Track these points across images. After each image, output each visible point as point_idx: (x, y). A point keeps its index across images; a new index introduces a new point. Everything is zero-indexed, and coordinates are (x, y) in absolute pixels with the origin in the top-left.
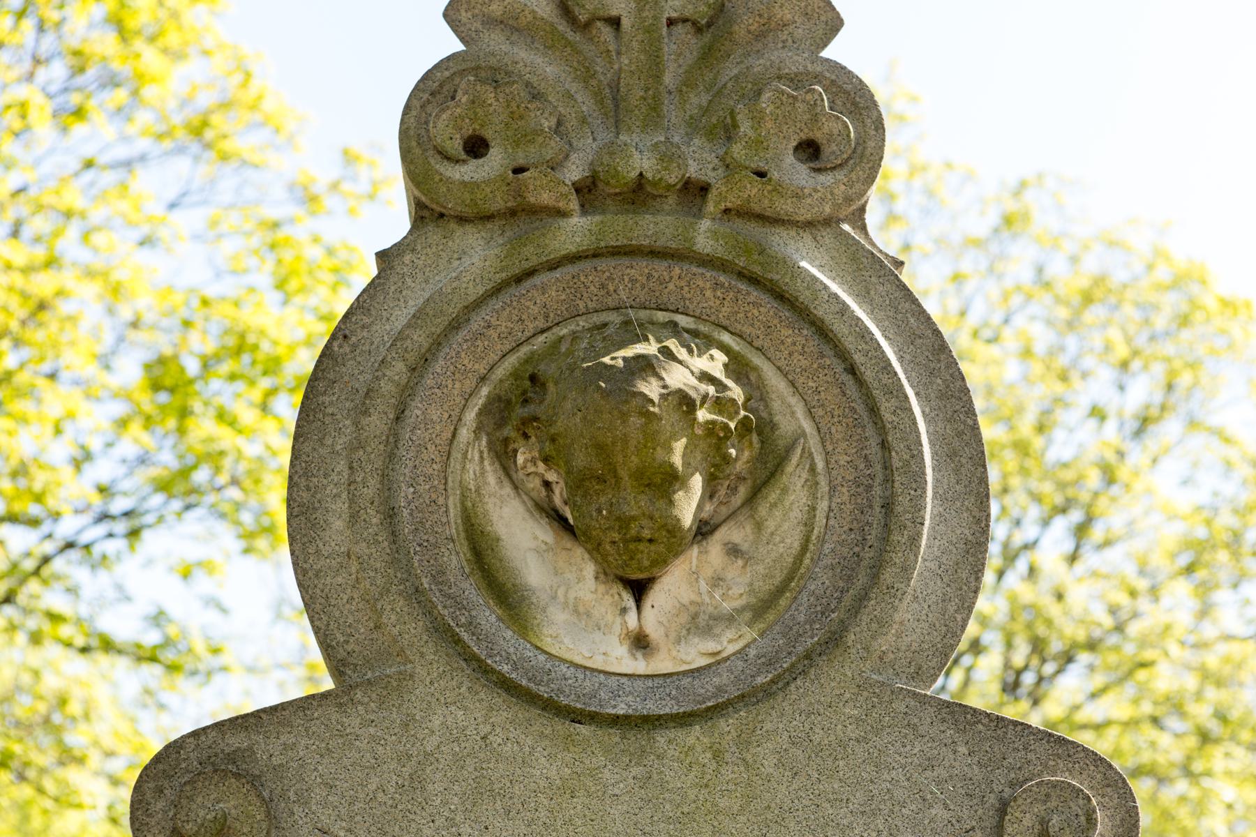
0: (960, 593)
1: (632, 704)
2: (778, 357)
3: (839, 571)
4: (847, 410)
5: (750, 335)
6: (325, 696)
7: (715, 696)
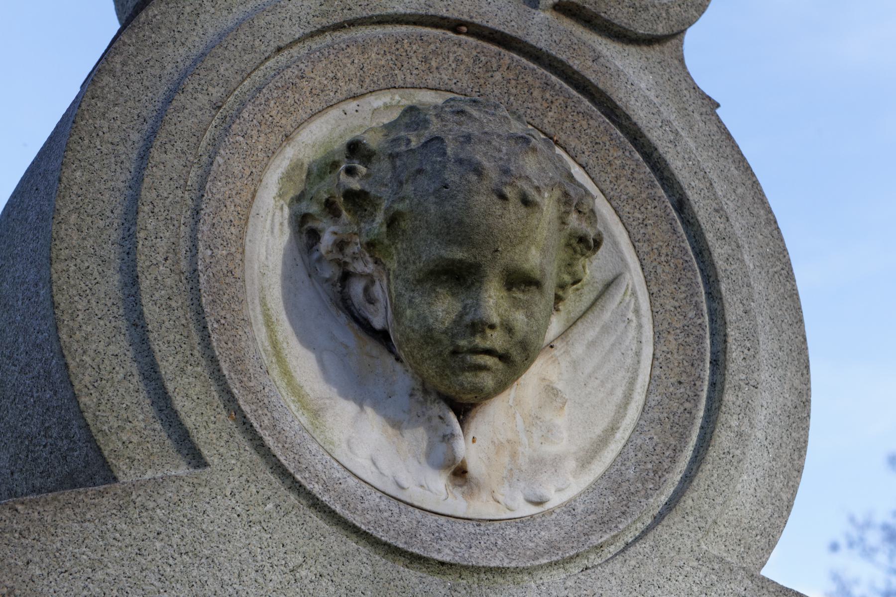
0: (784, 469)
1: (458, 550)
2: (603, 179)
3: (668, 426)
4: (676, 249)
5: (574, 149)
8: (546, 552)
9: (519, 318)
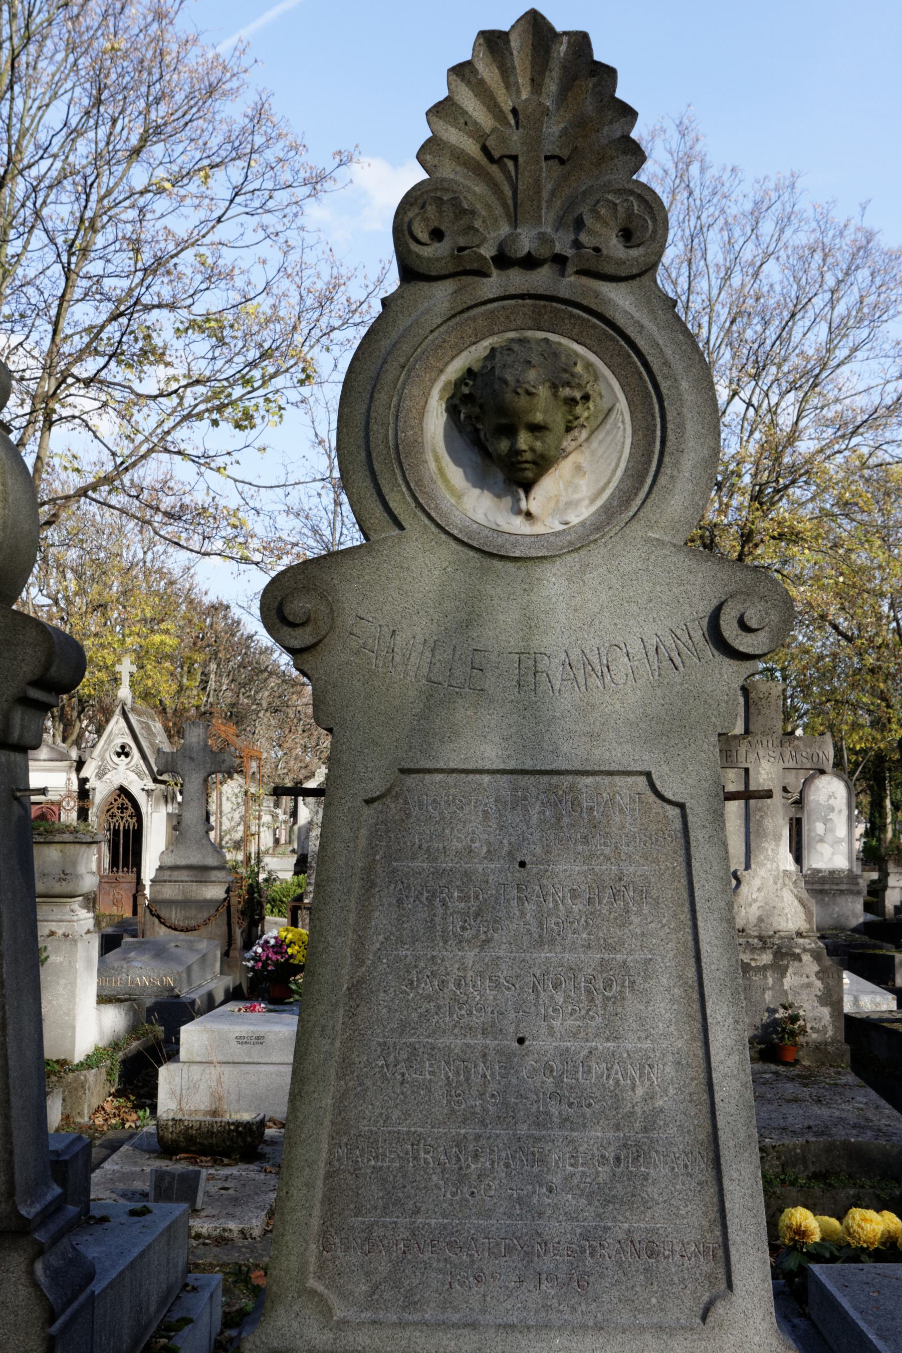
6: (360, 547)
7: (568, 546)
8: (568, 546)
9: (538, 445)
